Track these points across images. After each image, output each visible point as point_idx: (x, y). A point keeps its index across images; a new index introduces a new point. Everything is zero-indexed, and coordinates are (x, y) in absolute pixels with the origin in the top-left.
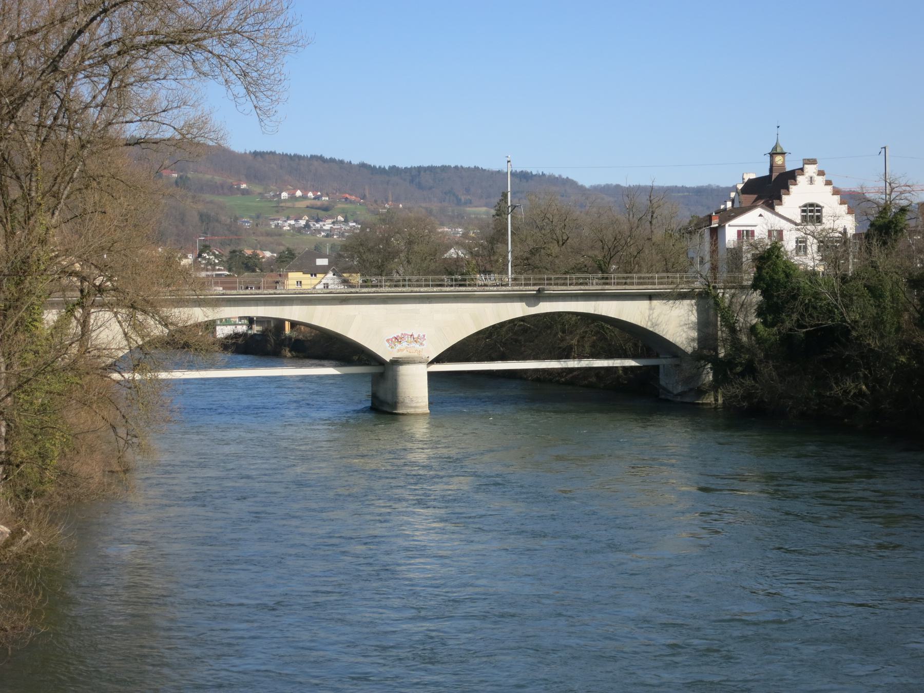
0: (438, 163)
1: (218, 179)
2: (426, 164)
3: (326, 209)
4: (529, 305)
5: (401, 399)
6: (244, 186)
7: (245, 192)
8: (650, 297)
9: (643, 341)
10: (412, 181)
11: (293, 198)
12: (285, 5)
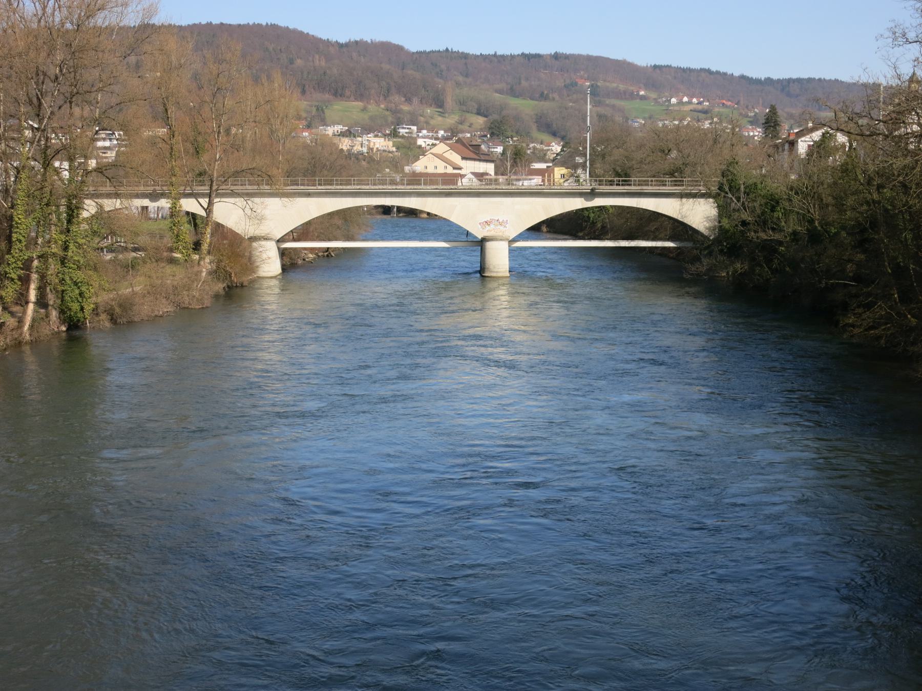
0: (805, 76)
1: (622, 87)
2: (795, 76)
3: (705, 112)
4: (587, 200)
5: (487, 266)
6: (642, 93)
7: (643, 98)
8: (681, 196)
9: (679, 229)
10: (782, 90)
11: (680, 103)
12: (15, 5)
